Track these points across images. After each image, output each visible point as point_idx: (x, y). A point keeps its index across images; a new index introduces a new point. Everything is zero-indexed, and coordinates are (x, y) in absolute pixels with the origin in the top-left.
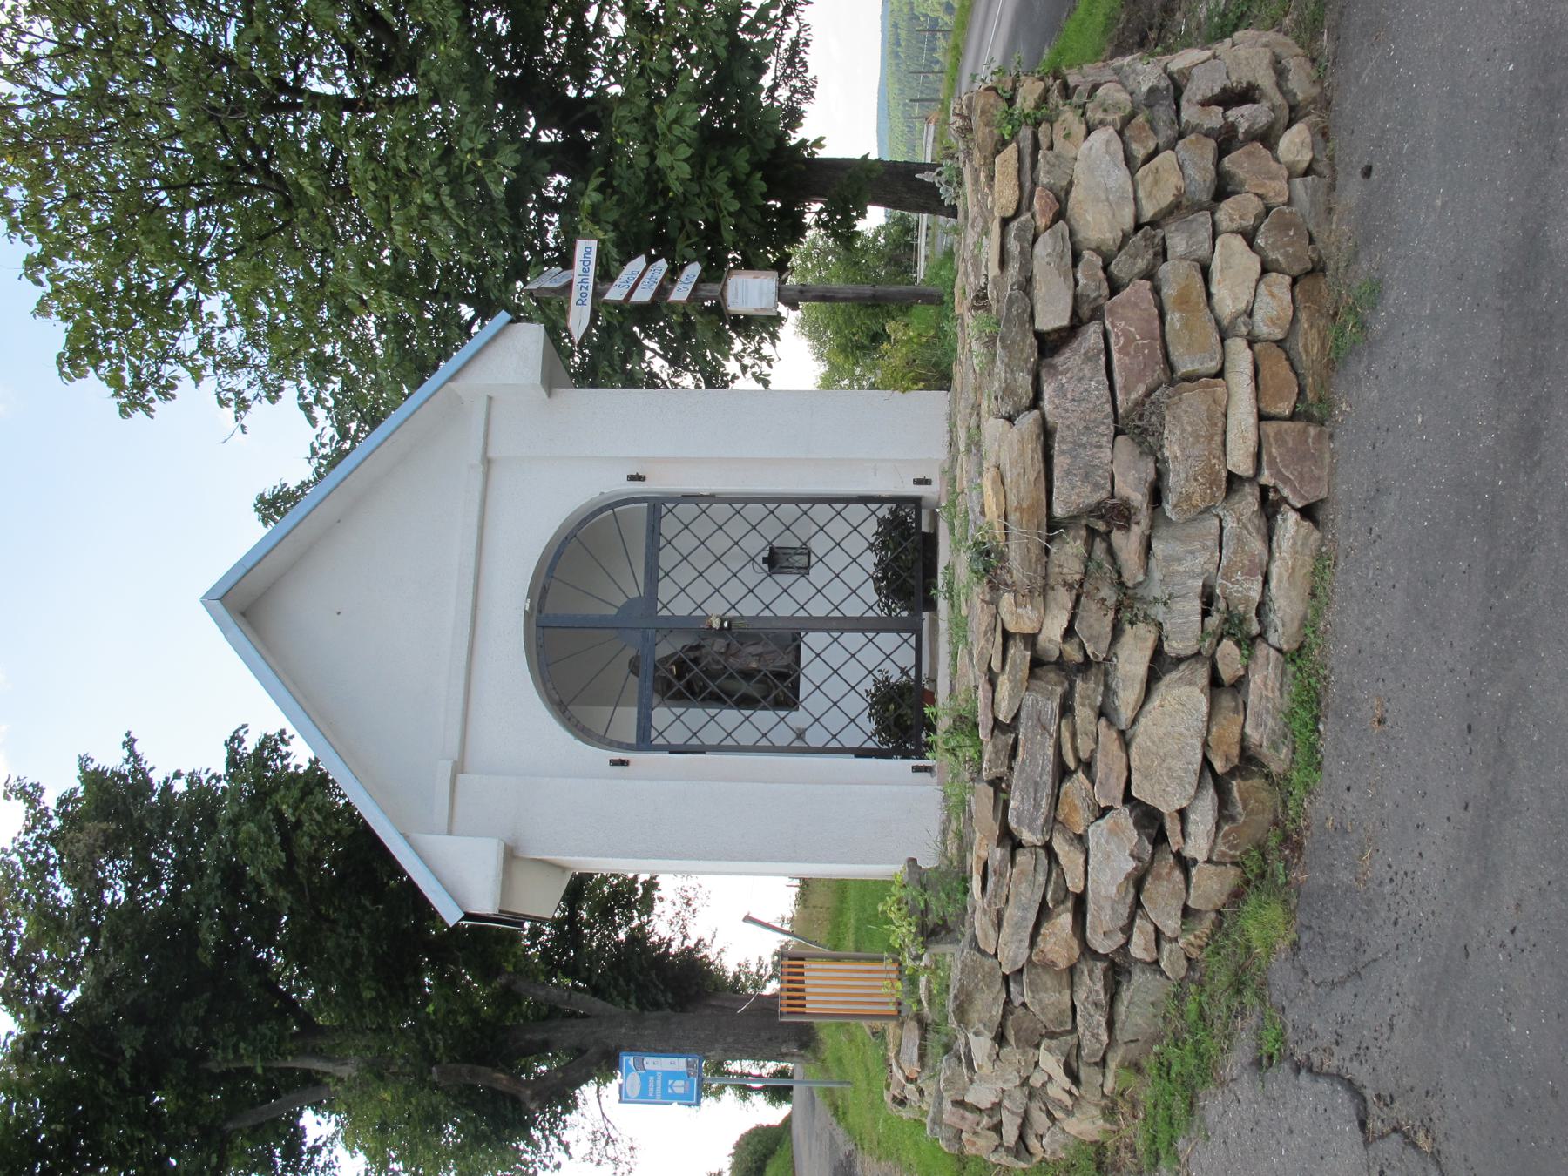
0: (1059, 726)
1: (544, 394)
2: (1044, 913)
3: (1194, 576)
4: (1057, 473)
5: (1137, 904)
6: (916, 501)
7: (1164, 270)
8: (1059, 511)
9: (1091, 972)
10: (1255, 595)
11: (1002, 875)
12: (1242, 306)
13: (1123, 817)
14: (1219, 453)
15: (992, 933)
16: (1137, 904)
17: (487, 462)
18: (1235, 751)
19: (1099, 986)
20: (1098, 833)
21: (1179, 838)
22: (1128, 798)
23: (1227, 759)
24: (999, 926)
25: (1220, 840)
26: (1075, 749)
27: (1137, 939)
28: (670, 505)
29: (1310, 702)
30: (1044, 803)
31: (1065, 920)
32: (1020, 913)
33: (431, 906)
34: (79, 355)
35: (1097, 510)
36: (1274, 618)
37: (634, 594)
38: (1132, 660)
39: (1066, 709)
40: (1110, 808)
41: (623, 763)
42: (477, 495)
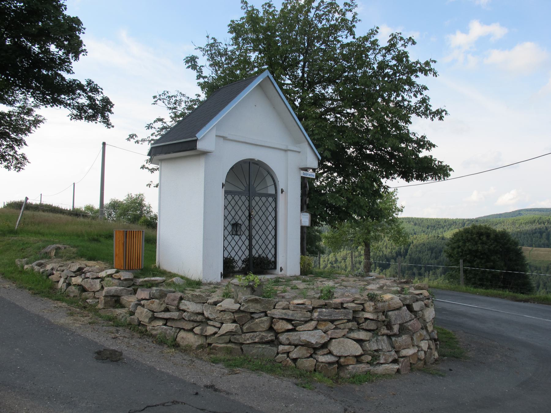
3: (382, 346)
5: (296, 346)
6: (275, 268)
8: (390, 313)
9: (272, 336)
10: (382, 361)
11: (304, 309)
13: (326, 339)
15: (281, 307)
16: (296, 346)
17: (286, 151)
18: (346, 364)
19: (269, 338)
20: (319, 332)
21: (322, 353)
22: (331, 339)
23: (344, 362)
24: (283, 309)
25: (323, 364)
27: (286, 347)
29: (356, 379)
30: (326, 318)
31: (290, 327)
32: (290, 314)
34: (252, 18)
35: (389, 322)
36: (377, 368)
37: (257, 189)
38: (362, 335)
39: (349, 321)
42: (280, 147)
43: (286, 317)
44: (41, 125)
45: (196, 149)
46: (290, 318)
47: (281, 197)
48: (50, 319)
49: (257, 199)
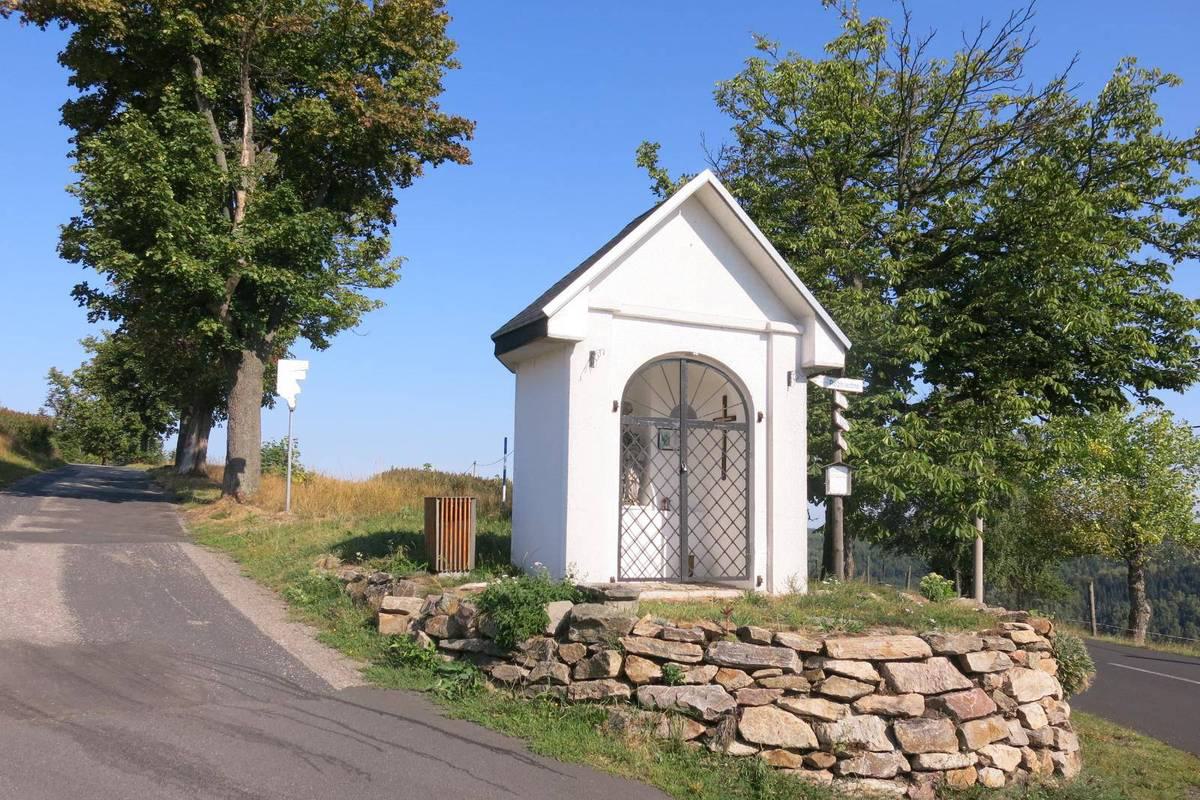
0: (778, 667)
1: (328, 349)
2: (659, 661)
4: (906, 664)
7: (1000, 717)
12: (996, 762)
14: (927, 749)
26: (765, 677)
28: (744, 436)
31: (657, 672)
33: (746, 290)
40: (735, 697)
41: (615, 409)
43: (651, 652)
44: (58, 370)
45: (546, 334)
46: (659, 654)
47: (759, 430)
48: (208, 575)
49: (700, 433)
